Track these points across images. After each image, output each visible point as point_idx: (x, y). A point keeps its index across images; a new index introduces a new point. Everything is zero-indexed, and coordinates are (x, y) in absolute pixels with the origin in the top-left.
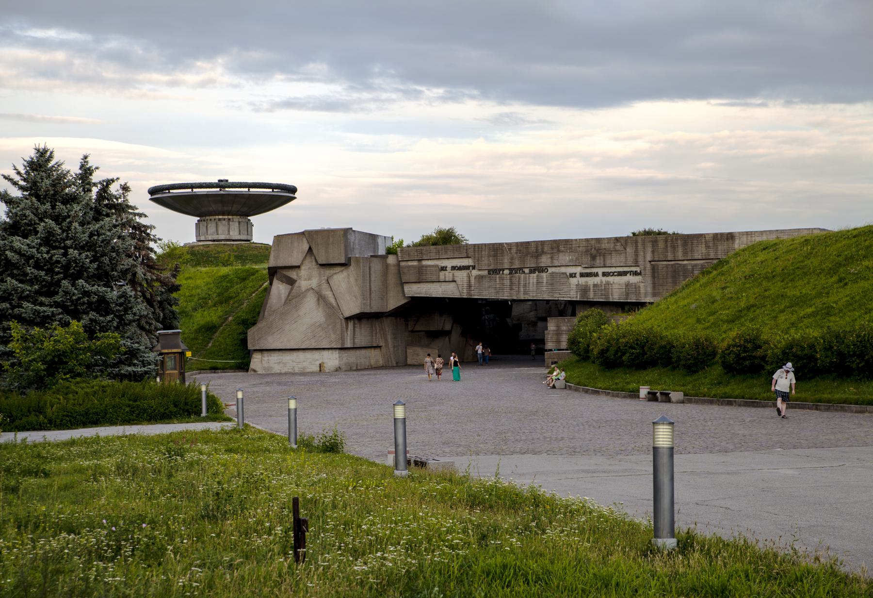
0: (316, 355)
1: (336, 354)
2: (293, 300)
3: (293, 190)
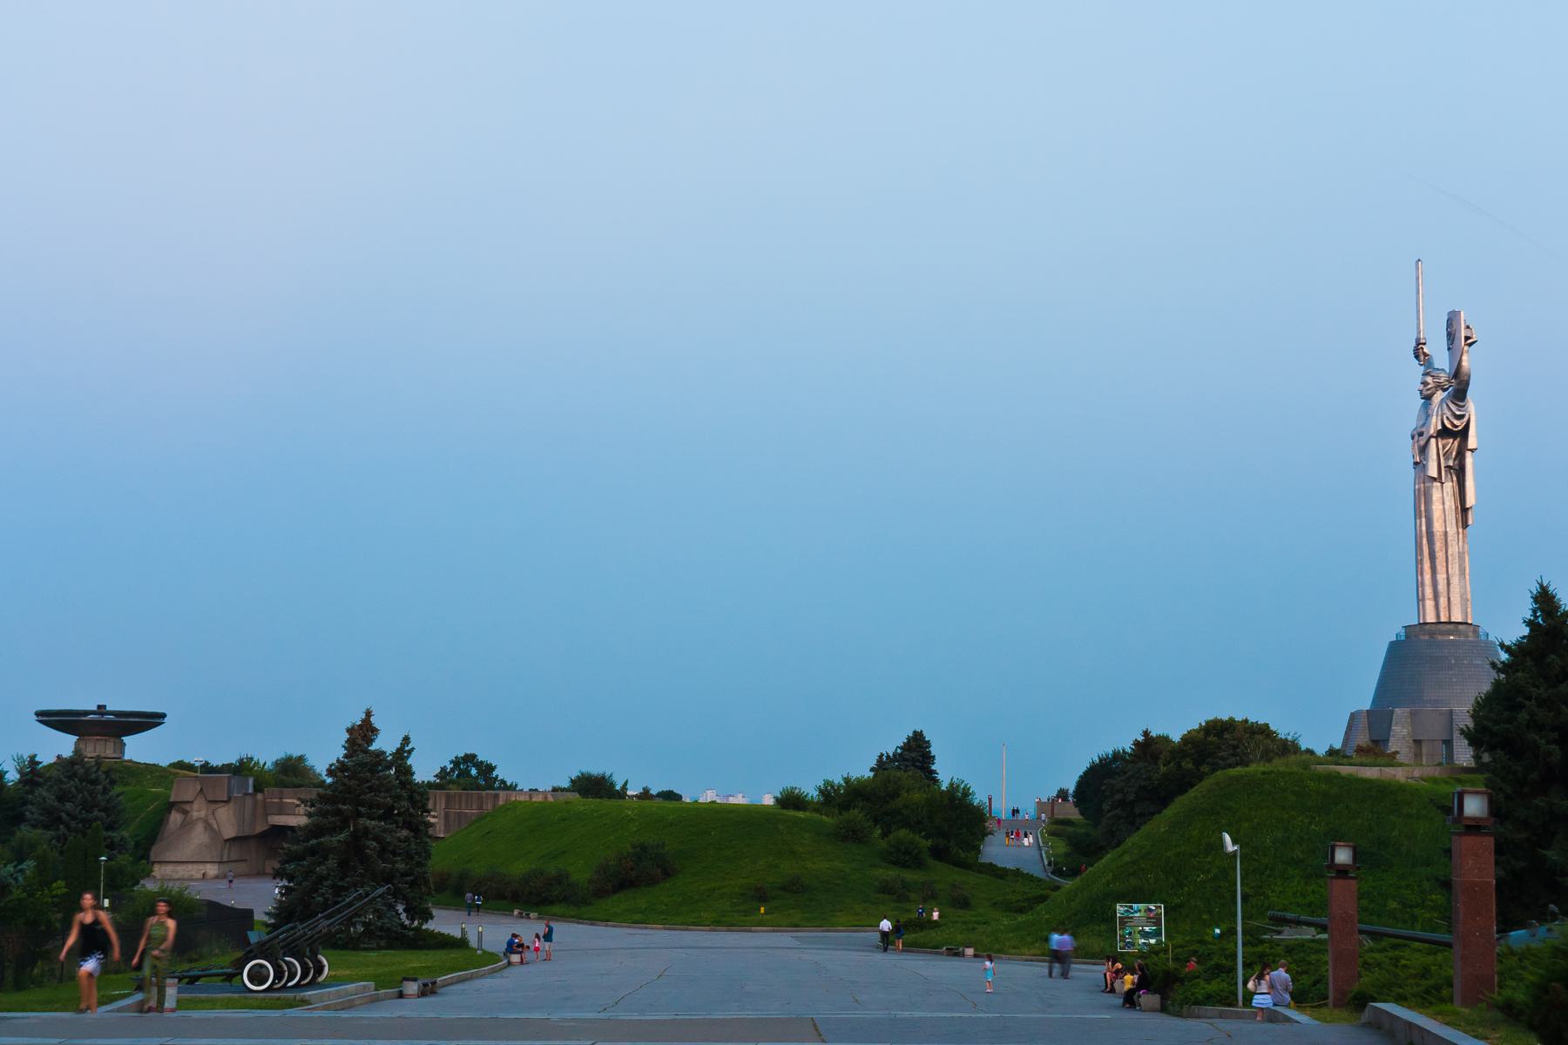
0: (201, 866)
1: (216, 867)
2: (187, 825)
3: (163, 716)
